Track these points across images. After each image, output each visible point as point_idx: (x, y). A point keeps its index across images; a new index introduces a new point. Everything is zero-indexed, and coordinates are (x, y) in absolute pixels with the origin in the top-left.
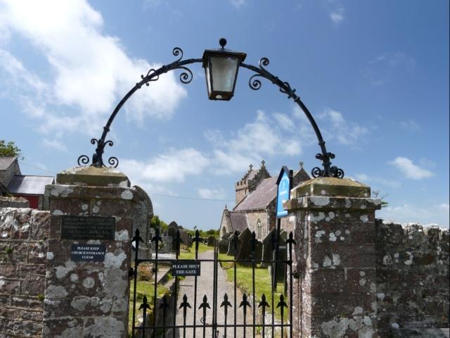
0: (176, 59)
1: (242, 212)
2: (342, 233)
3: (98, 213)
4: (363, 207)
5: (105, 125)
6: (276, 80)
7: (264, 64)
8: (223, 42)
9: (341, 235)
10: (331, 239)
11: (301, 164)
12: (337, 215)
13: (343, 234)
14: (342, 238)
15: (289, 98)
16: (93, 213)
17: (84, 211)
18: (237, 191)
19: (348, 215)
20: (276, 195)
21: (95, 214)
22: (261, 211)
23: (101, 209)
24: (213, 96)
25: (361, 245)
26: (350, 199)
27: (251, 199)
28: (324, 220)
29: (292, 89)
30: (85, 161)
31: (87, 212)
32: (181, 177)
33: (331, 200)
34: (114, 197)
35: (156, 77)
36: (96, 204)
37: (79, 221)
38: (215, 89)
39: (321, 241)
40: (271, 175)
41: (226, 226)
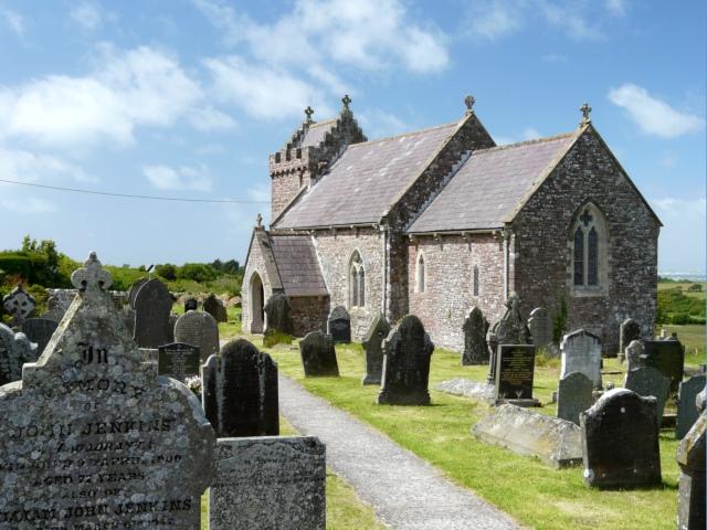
1: (301, 232)
11: (469, 102)
18: (273, 176)
22: (361, 229)
27: (316, 200)
32: (122, 131)
40: (365, 133)
41: (262, 272)
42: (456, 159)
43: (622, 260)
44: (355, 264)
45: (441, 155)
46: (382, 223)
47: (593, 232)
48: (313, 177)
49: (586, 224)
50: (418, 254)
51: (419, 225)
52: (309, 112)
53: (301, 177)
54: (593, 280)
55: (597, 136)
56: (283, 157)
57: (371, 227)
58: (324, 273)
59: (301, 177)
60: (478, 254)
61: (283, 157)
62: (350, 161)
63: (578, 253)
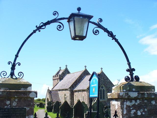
0: (54, 17)
1: (56, 91)
2: (143, 111)
3: (16, 106)
4: (153, 97)
5: (16, 54)
6: (106, 30)
7: (100, 21)
8: (79, 9)
9: (143, 112)
10: (138, 114)
11: (85, 67)
12: (141, 101)
13: (144, 111)
14: (143, 113)
15: (112, 39)
16: (13, 106)
17: (8, 105)
19: (146, 101)
20: (88, 85)
21: (15, 106)
23: (17, 104)
24: (74, 38)
25: (152, 116)
26: (147, 93)
28: (135, 104)
29: (114, 35)
30: (4, 74)
31: (9, 106)
33: (138, 94)
34: (26, 96)
35: (44, 27)
36: (15, 101)
37: (5, 111)
38: (77, 34)
39: (133, 116)
41: (49, 98)
42: (83, 77)
44: (65, 96)
45: (80, 76)
46: (69, 88)
47: (104, 90)
48: (60, 80)
49: (102, 88)
50: (76, 94)
51: (76, 89)
52: (60, 68)
53: (58, 80)
55: (104, 73)
56: (55, 76)
57: (67, 89)
58: (60, 98)
59: (58, 80)
61: (55, 76)
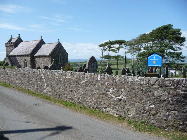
11: (59, 40)
43: (64, 59)
54: (60, 62)
60: (45, 59)
62: (21, 45)
63: (59, 58)
